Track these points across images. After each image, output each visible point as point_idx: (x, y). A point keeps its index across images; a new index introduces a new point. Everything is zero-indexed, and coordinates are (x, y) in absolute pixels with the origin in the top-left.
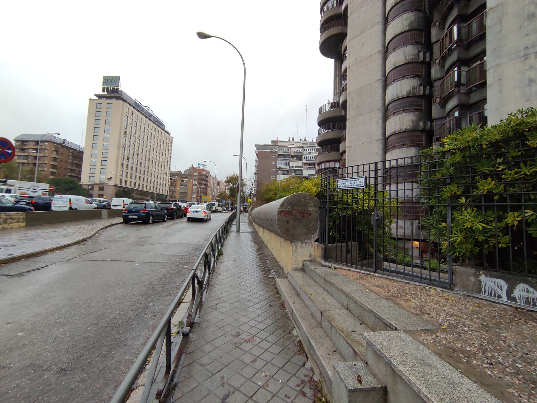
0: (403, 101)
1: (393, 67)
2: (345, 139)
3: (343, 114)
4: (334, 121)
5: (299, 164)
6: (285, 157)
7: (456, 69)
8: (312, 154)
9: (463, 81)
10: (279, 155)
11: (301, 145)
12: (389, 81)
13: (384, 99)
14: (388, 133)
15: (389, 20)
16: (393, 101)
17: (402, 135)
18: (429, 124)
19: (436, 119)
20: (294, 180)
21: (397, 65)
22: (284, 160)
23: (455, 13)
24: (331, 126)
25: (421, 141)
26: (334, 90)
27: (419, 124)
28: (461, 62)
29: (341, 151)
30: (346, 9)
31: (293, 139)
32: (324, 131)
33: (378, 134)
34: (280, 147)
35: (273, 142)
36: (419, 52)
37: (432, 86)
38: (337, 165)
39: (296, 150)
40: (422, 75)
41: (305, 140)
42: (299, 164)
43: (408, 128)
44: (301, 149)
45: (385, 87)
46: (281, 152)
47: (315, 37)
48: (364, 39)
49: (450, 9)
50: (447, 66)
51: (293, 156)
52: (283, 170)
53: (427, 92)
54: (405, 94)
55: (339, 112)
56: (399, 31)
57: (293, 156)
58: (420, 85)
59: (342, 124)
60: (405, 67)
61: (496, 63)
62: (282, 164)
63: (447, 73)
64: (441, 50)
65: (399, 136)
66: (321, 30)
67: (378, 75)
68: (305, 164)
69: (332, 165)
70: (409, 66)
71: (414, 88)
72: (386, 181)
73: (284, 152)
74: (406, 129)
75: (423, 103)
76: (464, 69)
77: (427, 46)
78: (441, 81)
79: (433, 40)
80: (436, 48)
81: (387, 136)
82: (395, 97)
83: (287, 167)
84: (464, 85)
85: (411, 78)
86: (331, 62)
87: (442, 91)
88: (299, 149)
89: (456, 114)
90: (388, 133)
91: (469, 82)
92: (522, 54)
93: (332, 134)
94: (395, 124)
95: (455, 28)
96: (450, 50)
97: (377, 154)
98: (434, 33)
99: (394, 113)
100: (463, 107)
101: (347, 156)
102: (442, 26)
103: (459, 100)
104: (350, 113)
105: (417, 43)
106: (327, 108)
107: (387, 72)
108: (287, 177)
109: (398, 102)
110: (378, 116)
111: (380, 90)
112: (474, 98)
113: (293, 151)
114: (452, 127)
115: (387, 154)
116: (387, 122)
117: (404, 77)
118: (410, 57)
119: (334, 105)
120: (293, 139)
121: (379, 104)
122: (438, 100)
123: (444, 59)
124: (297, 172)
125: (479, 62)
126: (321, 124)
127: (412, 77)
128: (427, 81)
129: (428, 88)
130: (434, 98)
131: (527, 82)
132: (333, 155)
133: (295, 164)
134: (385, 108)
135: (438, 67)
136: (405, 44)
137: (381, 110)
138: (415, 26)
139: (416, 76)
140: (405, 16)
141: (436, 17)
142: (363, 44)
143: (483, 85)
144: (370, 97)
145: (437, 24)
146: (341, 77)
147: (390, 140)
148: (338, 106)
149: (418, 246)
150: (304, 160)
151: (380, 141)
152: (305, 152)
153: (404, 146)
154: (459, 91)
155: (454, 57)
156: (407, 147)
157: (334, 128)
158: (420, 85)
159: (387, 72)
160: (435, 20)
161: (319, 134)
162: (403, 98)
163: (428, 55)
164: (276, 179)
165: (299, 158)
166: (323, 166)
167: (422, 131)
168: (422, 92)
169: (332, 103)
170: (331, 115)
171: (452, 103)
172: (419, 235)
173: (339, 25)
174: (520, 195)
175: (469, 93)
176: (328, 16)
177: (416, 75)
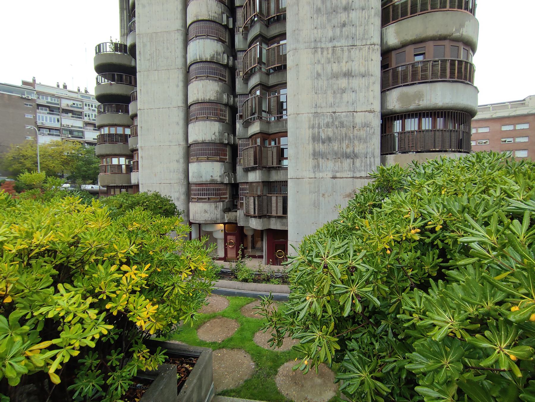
1: (195, 19)
2: (135, 99)
4: (119, 69)
5: (78, 123)
6: (52, 110)
7: (258, 43)
9: (264, 60)
10: (39, 105)
11: (80, 97)
14: (190, 101)
17: (206, 106)
18: (232, 99)
19: (239, 95)
20: (71, 145)
22: (48, 113)
24: (116, 77)
27: (222, 97)
29: (130, 113)
32: (105, 82)
34: (39, 93)
35: (24, 83)
36: (223, 13)
37: (235, 58)
38: (128, 131)
39: (70, 103)
40: (226, 42)
41: (86, 92)
42: (78, 123)
43: (212, 98)
44: (79, 103)
46: (42, 101)
51: (66, 111)
52: (50, 129)
57: (66, 111)
62: (46, 119)
63: (250, 46)
64: (245, 17)
68: (87, 124)
69: (120, 131)
71: (218, 54)
73: (48, 102)
75: (227, 74)
80: (240, 13)
81: (189, 104)
82: (198, 58)
83: (57, 125)
85: (214, 40)
87: (244, 67)
89: (258, 93)
90: (190, 101)
92: (313, 45)
99: (197, 77)
100: (266, 88)
101: (139, 121)
103: (261, 78)
104: (141, 64)
106: (109, 49)
108: (59, 139)
109: (201, 65)
110: (178, 76)
111: (179, 44)
113: (64, 104)
114: (254, 107)
115: (189, 126)
116: (189, 87)
118: (213, 15)
119: (119, 48)
123: (247, 29)
124: (76, 134)
125: (276, 45)
127: (216, 40)
130: (238, 70)
132: (120, 117)
133: (68, 121)
135: (241, 36)
143: (282, 68)
144: (168, 49)
149: (223, 228)
150: (86, 119)
153: (207, 119)
154: (261, 68)
155: (255, 31)
156: (212, 120)
157: (120, 80)
158: (224, 53)
161: (98, 83)
162: (206, 62)
163: (231, 20)
164: (36, 141)
165: (78, 115)
167: (226, 105)
170: (115, 61)
171: (254, 80)
172: (223, 218)
174: (62, 112)
177: (219, 38)
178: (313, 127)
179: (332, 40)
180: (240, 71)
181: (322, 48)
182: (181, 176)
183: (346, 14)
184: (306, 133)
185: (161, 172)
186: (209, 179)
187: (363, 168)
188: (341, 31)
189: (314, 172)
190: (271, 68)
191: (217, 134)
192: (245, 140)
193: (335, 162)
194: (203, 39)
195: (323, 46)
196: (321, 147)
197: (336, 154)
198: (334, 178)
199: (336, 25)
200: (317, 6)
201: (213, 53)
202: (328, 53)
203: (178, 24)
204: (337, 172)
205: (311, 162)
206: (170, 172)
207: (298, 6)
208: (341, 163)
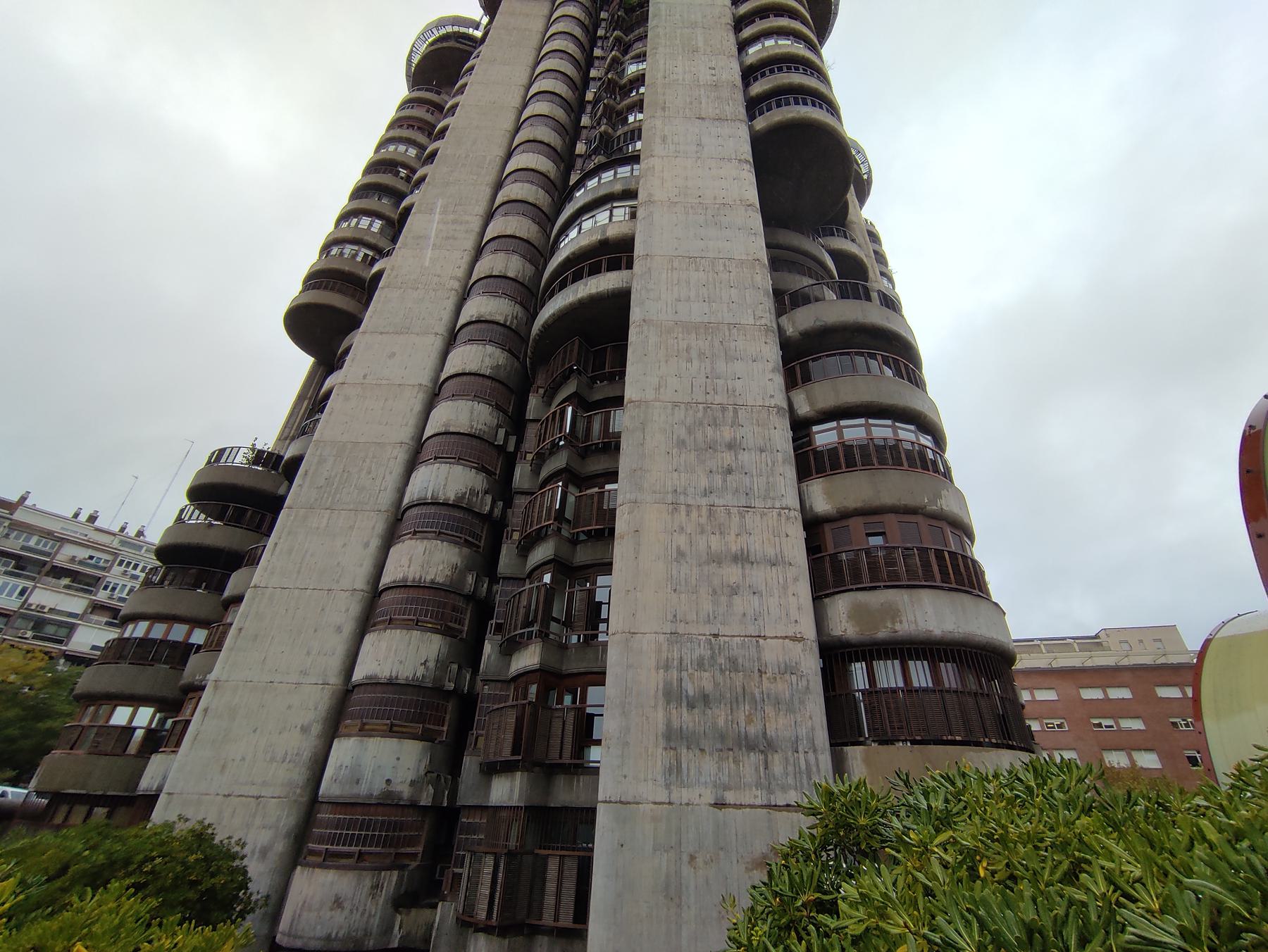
0: (444, 511)
1: (443, 430)
3: (281, 491)
4: (243, 500)
8: (122, 584)
9: (569, 514)
11: (116, 544)
12: (424, 456)
13: (401, 492)
14: (386, 580)
15: (458, 342)
16: (421, 503)
19: (504, 578)
21: (452, 429)
23: (569, 389)
24: (230, 512)
25: (461, 623)
26: (285, 426)
28: (570, 476)
29: (227, 594)
30: (379, 275)
31: (92, 519)
32: (197, 518)
33: (358, 576)
36: (499, 426)
37: (508, 504)
39: (83, 554)
41: (140, 533)
42: (76, 604)
43: (440, 579)
44: (105, 556)
45: (411, 466)
47: (288, 287)
48: (398, 346)
49: (565, 378)
50: (544, 473)
51: (58, 572)
53: (497, 512)
54: (451, 496)
55: (263, 480)
56: (472, 367)
57: (58, 572)
58: (486, 492)
59: (269, 518)
60: (465, 440)
61: (633, 497)
64: (541, 438)
65: (413, 594)
66: (305, 282)
67: (404, 432)
68: (97, 608)
69: (178, 632)
70: (475, 442)
71: (473, 492)
72: (301, 848)
74: (433, 582)
76: (573, 492)
77: (517, 423)
78: (529, 498)
79: (530, 414)
80: (531, 432)
82: (429, 495)
84: (568, 521)
86: (304, 362)
88: (97, 554)
89: (547, 578)
91: (575, 522)
92: (670, 498)
93: (220, 535)
94: (410, 560)
95: (570, 409)
96: (554, 448)
97: (339, 629)
98: (533, 402)
99: (415, 533)
102: (549, 397)
103: (556, 550)
104: (298, 493)
105: (498, 407)
106: (240, 460)
107: (428, 433)
109: (433, 509)
110: (373, 526)
111: (397, 467)
112: (583, 555)
113: (65, 556)
114: (533, 607)
117: (459, 460)
120: (92, 519)
121: (386, 499)
122: (516, 536)
123: (541, 458)
124: (50, 630)
125: (596, 490)
126: (199, 494)
128: (503, 489)
129: (500, 504)
131: (674, 555)
132: (197, 600)
134: (396, 515)
136: (477, 397)
137: (385, 516)
138: (502, 375)
139: (482, 469)
140: (490, 349)
141: (540, 380)
142: (393, 355)
145: (541, 391)
146: (313, 402)
147: (386, 597)
148: (275, 467)
150: (102, 596)
151: (359, 596)
152: (117, 569)
154: (559, 529)
155: (558, 462)
157: (236, 520)
158: (486, 492)
159: (428, 433)
160: (539, 382)
161: (179, 519)
165: (81, 580)
166: (139, 630)
167: (469, 598)
168: (488, 508)
169: (261, 452)
171: (542, 552)
173: (353, 296)
175: (574, 541)
176: (335, 265)
178: (667, 667)
179: (707, 492)
182: (299, 775)
184: (651, 680)
185: (243, 759)
186: (378, 787)
187: (790, 781)
189: (668, 786)
191: (431, 664)
192: (499, 685)
193: (721, 759)
195: (690, 501)
196: (686, 719)
197: (723, 737)
198: (720, 805)
204: (726, 788)
205: (660, 757)
206: (273, 759)
208: (736, 762)
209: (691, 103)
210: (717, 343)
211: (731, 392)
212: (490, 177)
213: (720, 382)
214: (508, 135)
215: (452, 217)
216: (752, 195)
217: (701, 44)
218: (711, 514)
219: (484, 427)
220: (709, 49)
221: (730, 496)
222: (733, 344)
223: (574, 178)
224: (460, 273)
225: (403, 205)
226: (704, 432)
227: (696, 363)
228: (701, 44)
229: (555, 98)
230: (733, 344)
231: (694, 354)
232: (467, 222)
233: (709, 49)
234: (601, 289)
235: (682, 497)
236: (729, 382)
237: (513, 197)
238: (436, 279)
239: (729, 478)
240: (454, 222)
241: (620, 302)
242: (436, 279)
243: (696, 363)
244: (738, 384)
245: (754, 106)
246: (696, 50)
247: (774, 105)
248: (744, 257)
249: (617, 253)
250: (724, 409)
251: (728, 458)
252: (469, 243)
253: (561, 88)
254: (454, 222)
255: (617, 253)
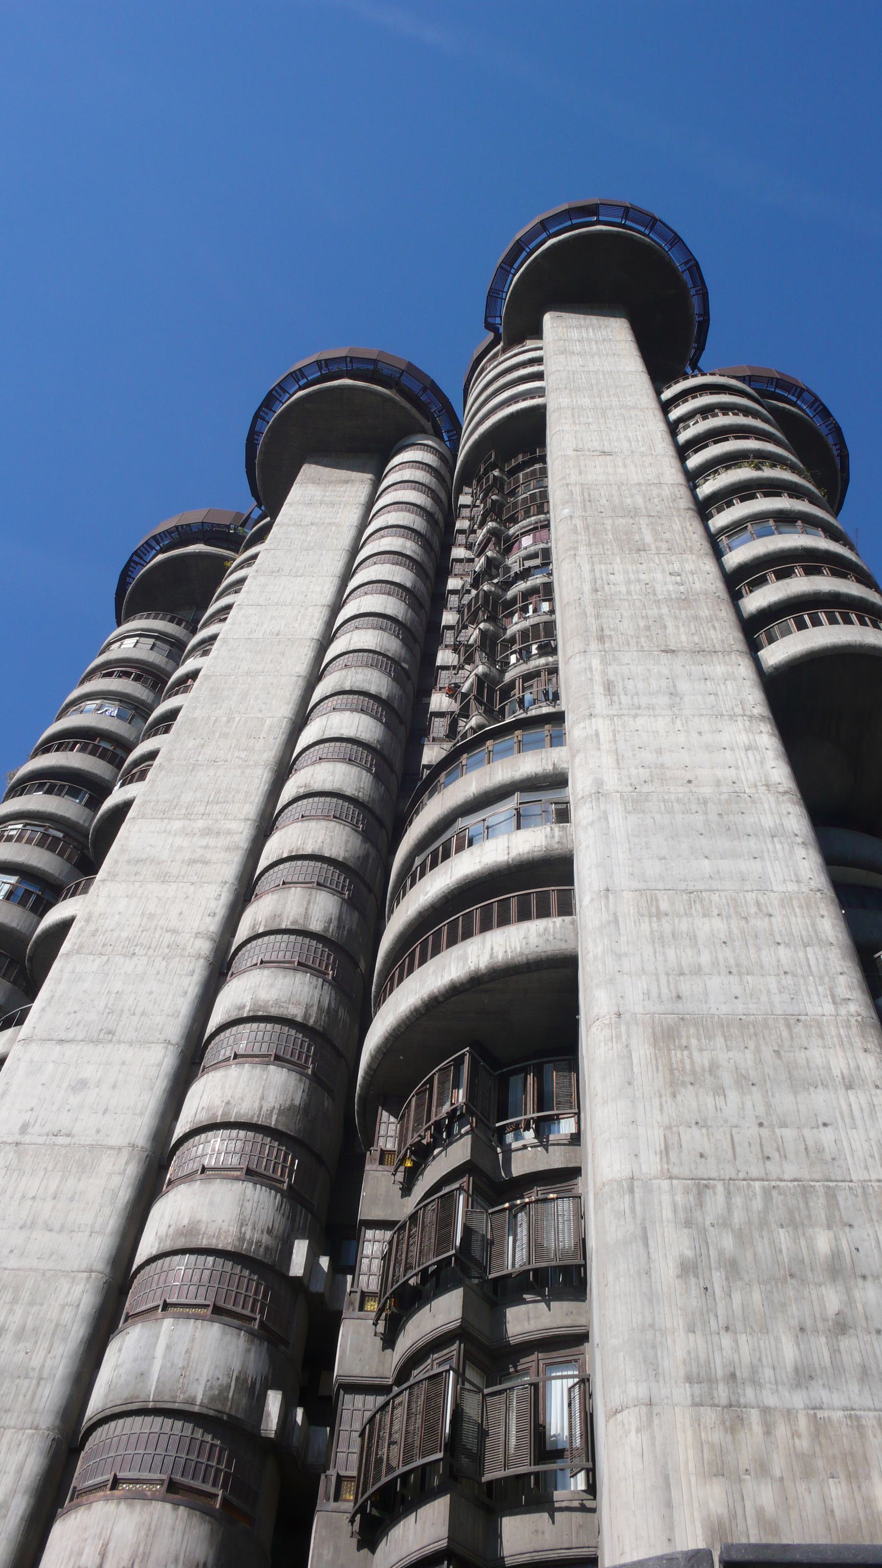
45: (109, 1317)
49: (443, 1134)
78: (381, 1400)
92: (722, 1393)
179: (803, 1376)
180: (340, 1478)
181: (766, 1411)
183: (566, 1142)
188: (835, 1351)
190: (532, 1118)
194: (197, 1318)
195: (770, 1400)
199: (809, 1323)
200: (721, 1253)
201: (224, 1381)
202: (795, 1434)
203: (94, 1247)
207: (646, 1245)
209: (648, 628)
210: (767, 1054)
211: (814, 1154)
212: (267, 751)
213: (788, 1134)
214: (301, 683)
215: (200, 824)
216: (779, 772)
217: (648, 538)
218: (819, 1428)
219: (265, 1239)
220: (664, 546)
221: (854, 1387)
222: (801, 1056)
223: (431, 754)
224: (213, 925)
225: (109, 803)
226: (773, 1243)
227: (733, 1096)
228: (648, 538)
229: (374, 559)
230: (801, 1056)
231: (727, 1078)
232: (229, 833)
233: (664, 546)
234: (514, 854)
235: (750, 1392)
236: (807, 1132)
237: (317, 786)
238: (168, 938)
239: (845, 1343)
240: (207, 832)
241: (554, 983)
242: (168, 938)
243: (733, 1096)
244: (827, 1136)
245: (755, 629)
246: (641, 549)
247: (763, 638)
248: (792, 887)
249: (544, 883)
250: (806, 1191)
251: (832, 1300)
252: (228, 869)
253: (392, 605)
254: (207, 832)
255: (544, 883)
